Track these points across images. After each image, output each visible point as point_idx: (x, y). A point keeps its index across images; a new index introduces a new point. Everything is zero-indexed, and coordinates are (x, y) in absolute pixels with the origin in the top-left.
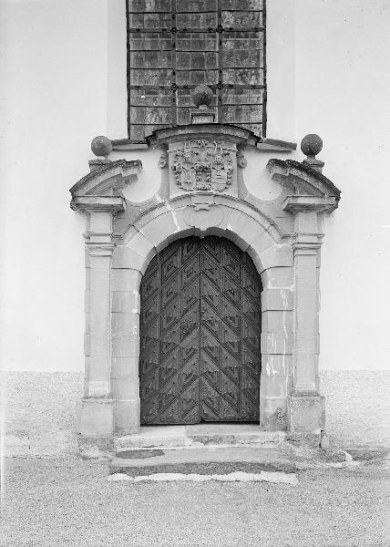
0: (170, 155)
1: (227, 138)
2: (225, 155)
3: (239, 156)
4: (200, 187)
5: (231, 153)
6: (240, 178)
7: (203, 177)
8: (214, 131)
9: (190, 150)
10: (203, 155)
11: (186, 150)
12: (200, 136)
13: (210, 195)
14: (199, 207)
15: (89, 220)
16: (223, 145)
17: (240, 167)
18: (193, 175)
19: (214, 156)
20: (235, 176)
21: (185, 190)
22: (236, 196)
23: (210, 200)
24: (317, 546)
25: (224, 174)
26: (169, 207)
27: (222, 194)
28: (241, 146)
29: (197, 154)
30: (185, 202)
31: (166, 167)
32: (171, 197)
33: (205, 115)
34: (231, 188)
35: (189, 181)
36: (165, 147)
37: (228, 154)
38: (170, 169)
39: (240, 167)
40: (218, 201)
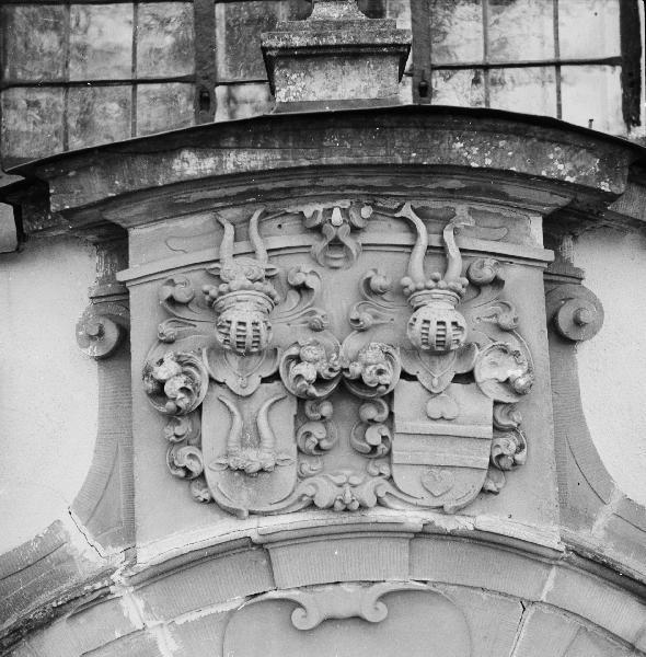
0: (137, 296)
1: (486, 187)
2: (477, 286)
3: (560, 280)
4: (325, 496)
5: (512, 274)
6: (568, 415)
7: (333, 429)
8: (400, 150)
9: (261, 264)
10: (336, 293)
11: (237, 271)
12: (320, 181)
13: (392, 532)
14: (318, 606)
15: (301, 296)
16: (468, 232)
17: (561, 338)
18: (278, 427)
19: (407, 298)
20: (536, 417)
21: (233, 513)
22: (549, 535)
23: (394, 567)
24: (282, 12)
25: (472, 409)
26: (133, 607)
27: (464, 524)
28: (559, 227)
29: (302, 289)
30: (229, 591)
31: (118, 353)
32: (151, 552)
33: (353, 54)
34: (512, 490)
35: (253, 459)
36: (114, 243)
37: (497, 283)
38: (140, 386)
39: (561, 338)
40: (433, 564)
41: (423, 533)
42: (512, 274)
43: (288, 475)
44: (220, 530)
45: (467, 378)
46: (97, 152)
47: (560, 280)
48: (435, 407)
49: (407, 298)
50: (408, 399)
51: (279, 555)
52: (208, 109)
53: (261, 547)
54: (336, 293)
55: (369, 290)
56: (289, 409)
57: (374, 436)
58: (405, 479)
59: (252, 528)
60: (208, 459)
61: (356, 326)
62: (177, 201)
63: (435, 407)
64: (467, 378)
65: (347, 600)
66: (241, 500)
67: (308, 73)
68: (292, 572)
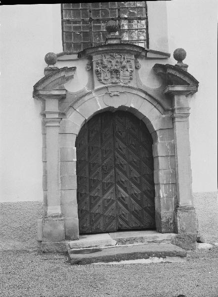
1: (129, 52)
2: (128, 62)
3: (136, 62)
5: (131, 61)
11: (105, 60)
13: (120, 86)
14: (113, 94)
18: (109, 75)
21: (104, 84)
23: (120, 90)
25: (128, 74)
26: (94, 94)
30: (104, 92)
32: (96, 88)
35: (106, 78)
40: (123, 90)
41: (123, 86)
42: (131, 61)
43: (110, 80)
44: (103, 86)
45: (127, 70)
46: (153, 197)
47: (136, 62)
48: (124, 73)
49: (121, 63)
50: (121, 72)
51: (109, 88)
52: (173, 138)
53: (107, 87)
54: (114, 62)
55: (117, 62)
56: (110, 73)
57: (118, 76)
58: (122, 81)
59: (106, 85)
60: (102, 78)
61: (116, 65)
62: (98, 53)
63: (124, 73)
64: (127, 70)
65: (116, 93)
66: (105, 82)
67: (154, 79)
68: (110, 90)
